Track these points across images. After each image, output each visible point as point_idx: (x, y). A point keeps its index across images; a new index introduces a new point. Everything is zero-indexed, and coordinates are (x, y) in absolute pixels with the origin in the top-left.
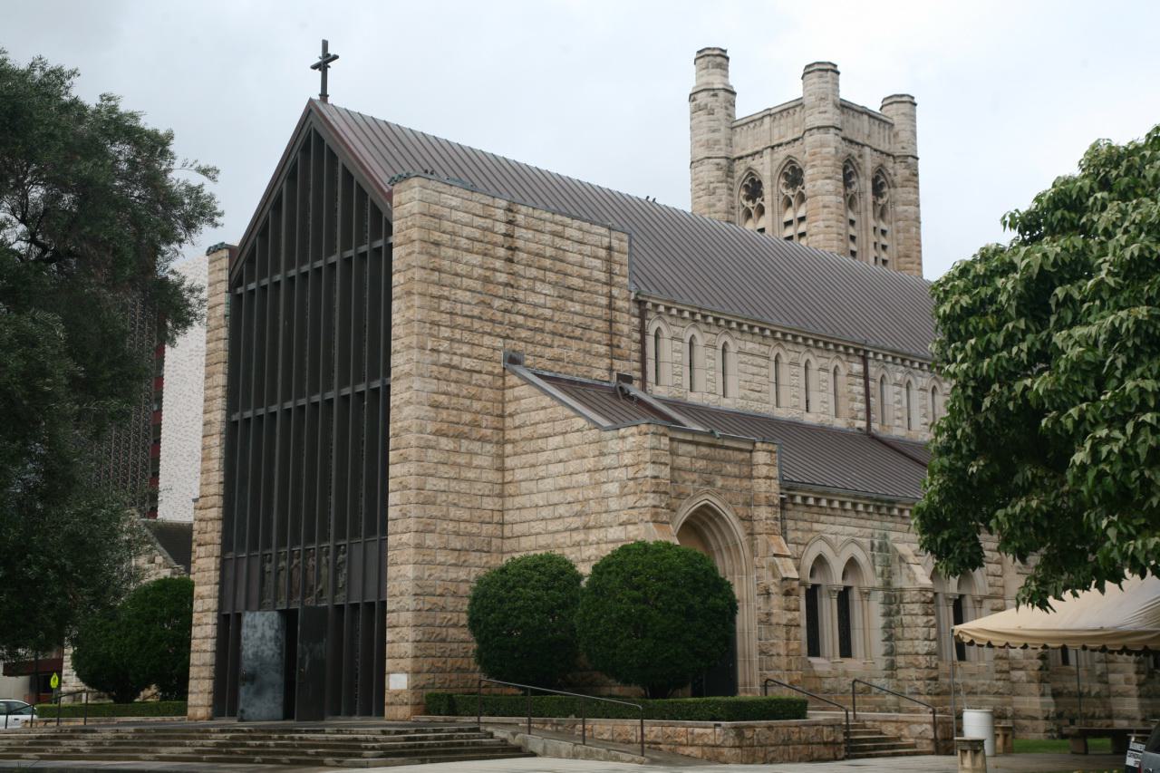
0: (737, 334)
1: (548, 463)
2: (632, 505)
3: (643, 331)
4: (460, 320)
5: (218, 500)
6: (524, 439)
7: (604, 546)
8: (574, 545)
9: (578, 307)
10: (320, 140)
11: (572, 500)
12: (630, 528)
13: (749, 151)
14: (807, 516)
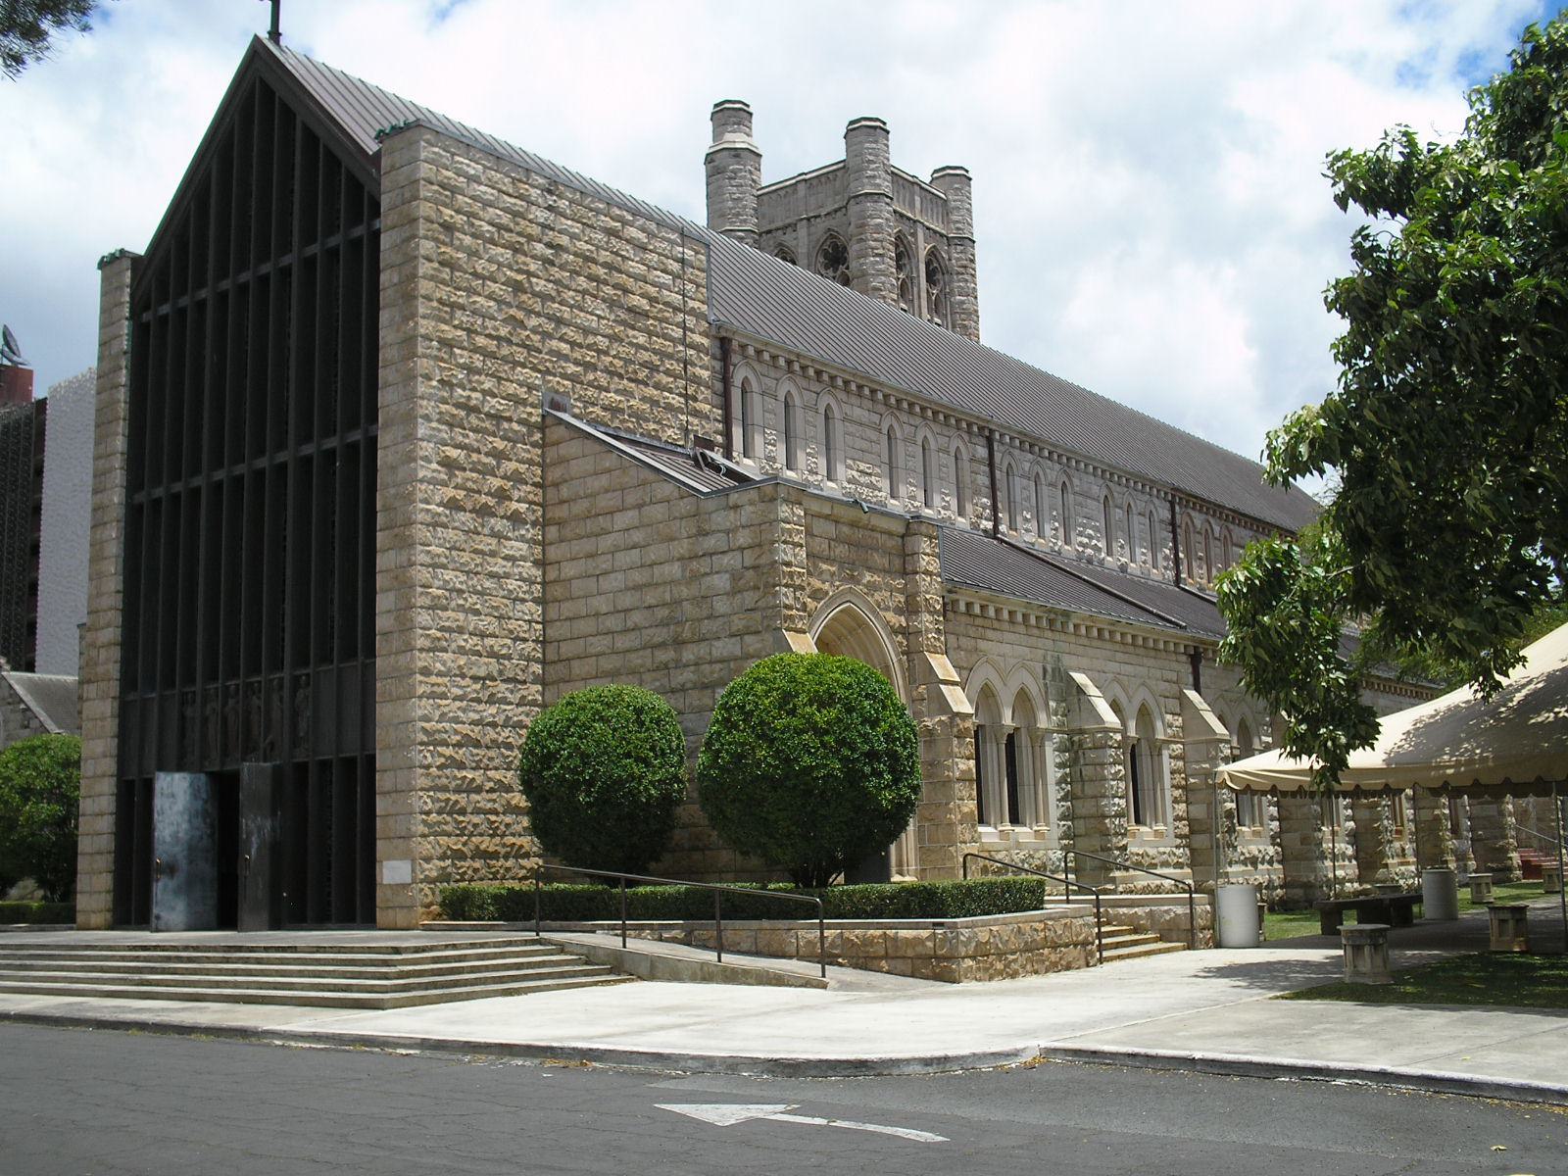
0: (842, 396)
1: (614, 551)
2: (753, 606)
3: (726, 379)
4: (481, 341)
5: (116, 618)
6: (578, 518)
7: (706, 668)
8: (658, 669)
9: (642, 339)
10: (268, 93)
11: (653, 602)
12: (748, 639)
13: (780, 224)
14: (972, 631)
